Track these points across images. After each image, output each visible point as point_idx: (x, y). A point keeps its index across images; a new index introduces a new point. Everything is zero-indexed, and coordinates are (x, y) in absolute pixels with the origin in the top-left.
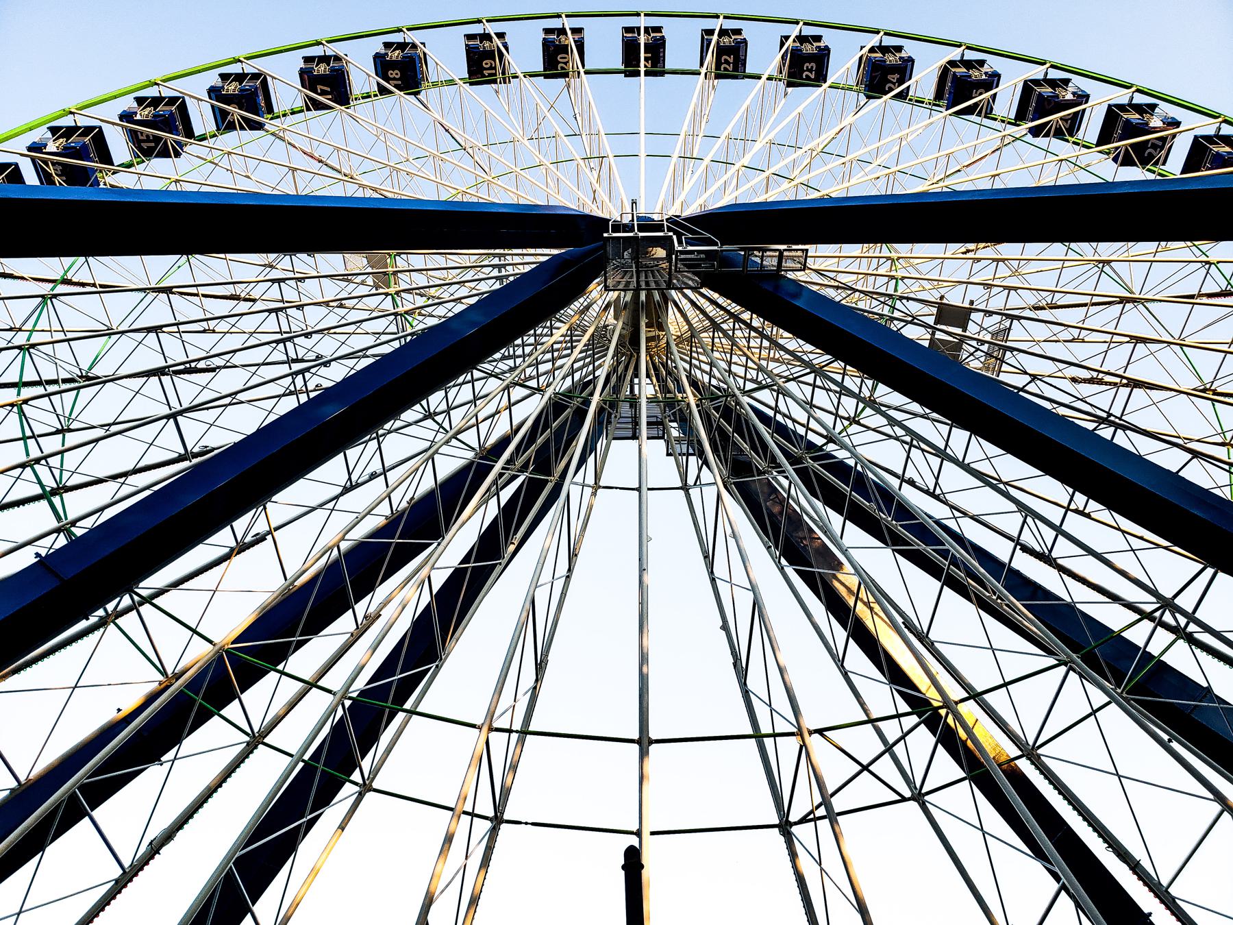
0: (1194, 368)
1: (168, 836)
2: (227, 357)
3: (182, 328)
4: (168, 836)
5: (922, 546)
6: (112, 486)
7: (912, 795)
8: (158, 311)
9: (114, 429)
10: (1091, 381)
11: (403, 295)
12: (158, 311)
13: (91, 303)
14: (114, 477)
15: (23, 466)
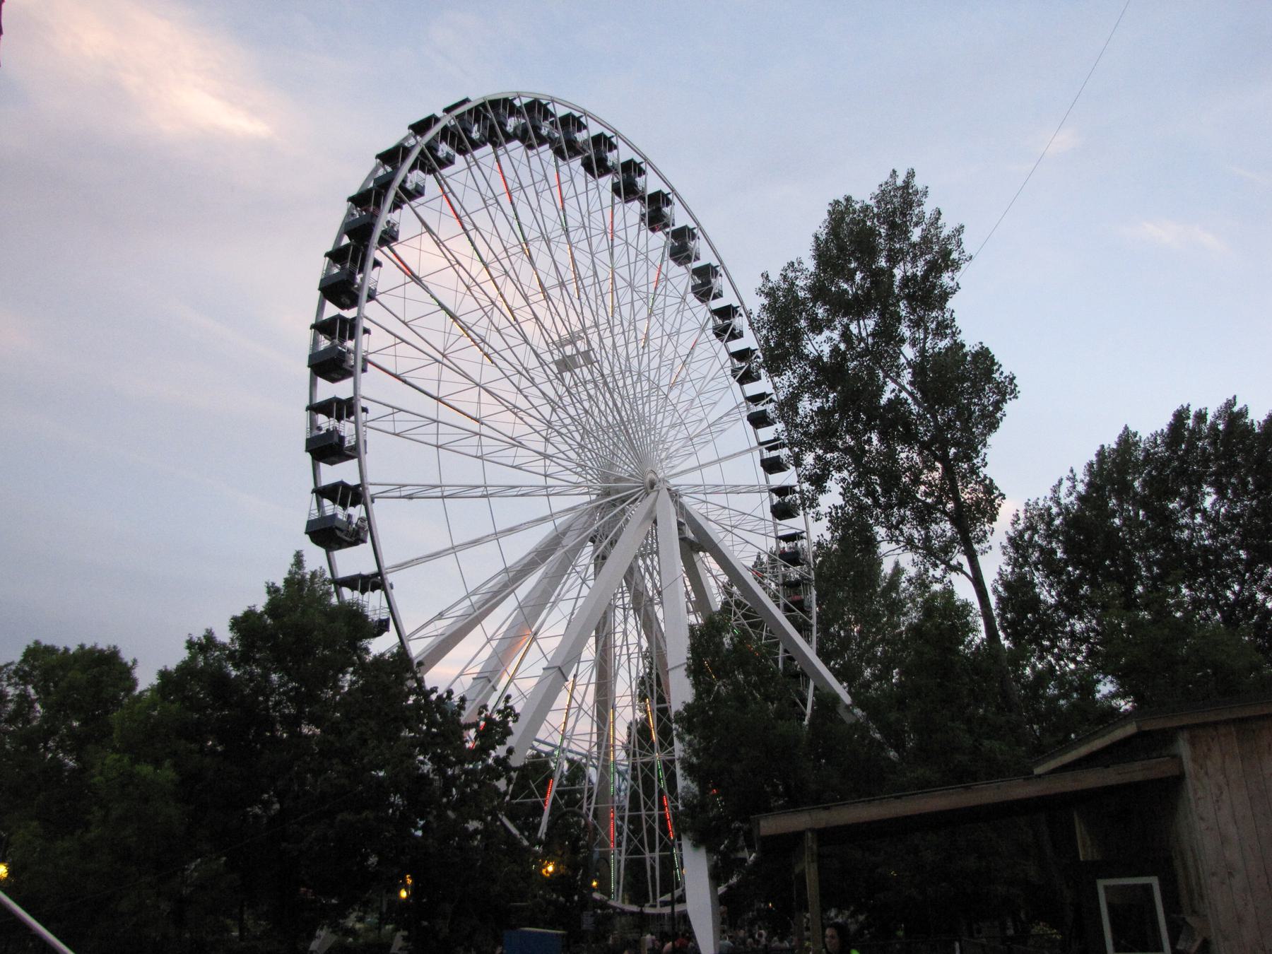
0: (456, 366)
1: (405, 382)
2: (587, 303)
3: (597, 285)
4: (405, 382)
5: (642, 796)
6: (512, 214)
7: (428, 691)
8: (604, 273)
9: (538, 216)
10: (550, 299)
11: (630, 652)
12: (604, 273)
13: (604, 245)
14: (516, 215)
15: (520, 184)
